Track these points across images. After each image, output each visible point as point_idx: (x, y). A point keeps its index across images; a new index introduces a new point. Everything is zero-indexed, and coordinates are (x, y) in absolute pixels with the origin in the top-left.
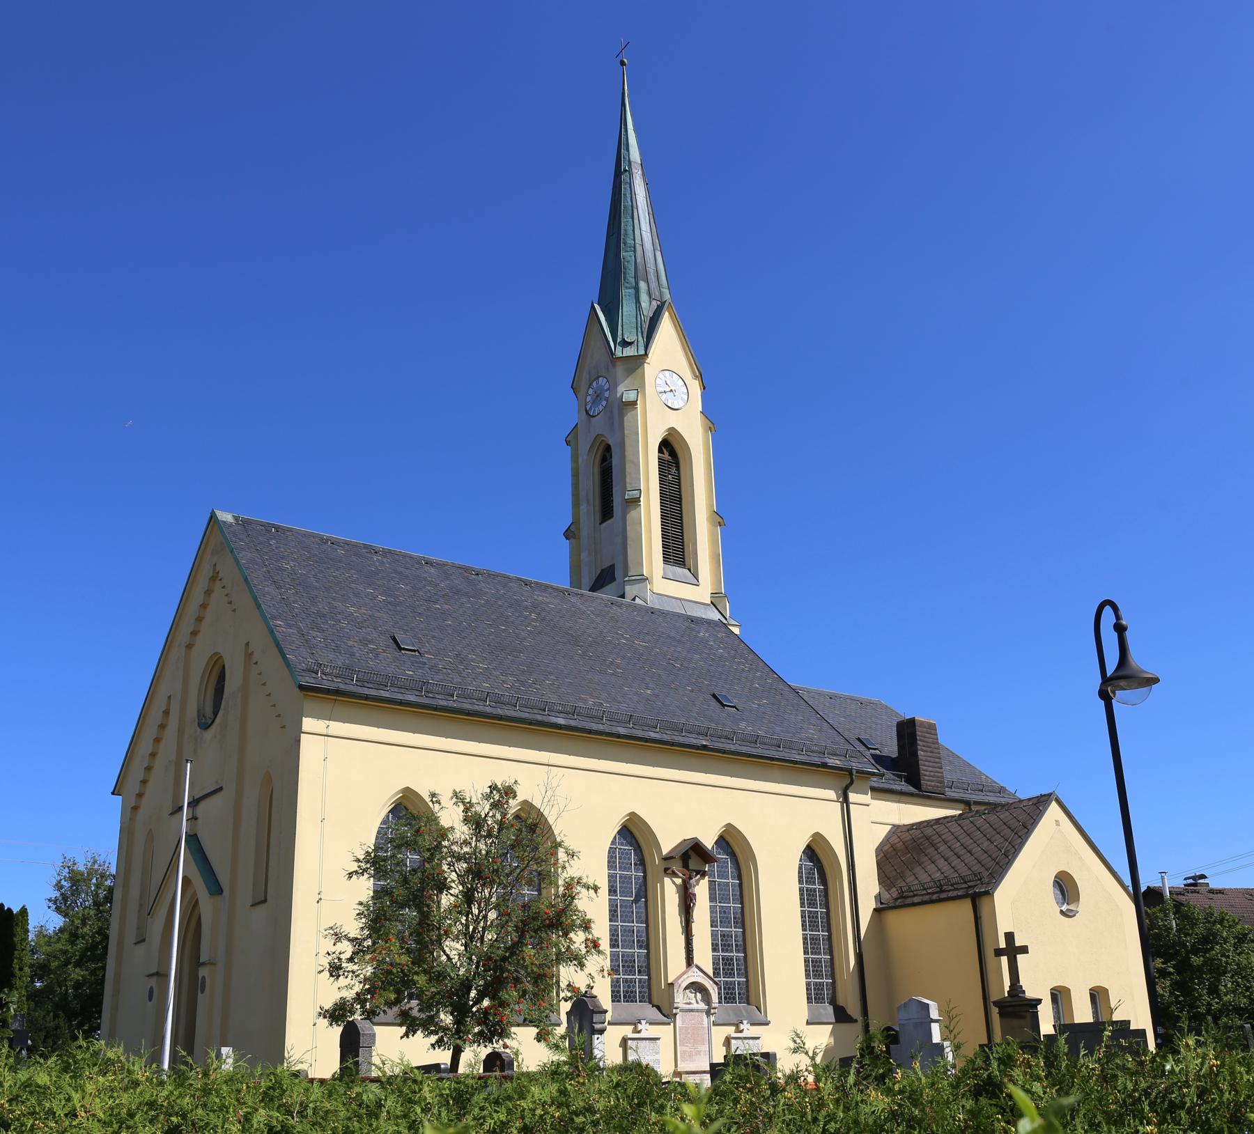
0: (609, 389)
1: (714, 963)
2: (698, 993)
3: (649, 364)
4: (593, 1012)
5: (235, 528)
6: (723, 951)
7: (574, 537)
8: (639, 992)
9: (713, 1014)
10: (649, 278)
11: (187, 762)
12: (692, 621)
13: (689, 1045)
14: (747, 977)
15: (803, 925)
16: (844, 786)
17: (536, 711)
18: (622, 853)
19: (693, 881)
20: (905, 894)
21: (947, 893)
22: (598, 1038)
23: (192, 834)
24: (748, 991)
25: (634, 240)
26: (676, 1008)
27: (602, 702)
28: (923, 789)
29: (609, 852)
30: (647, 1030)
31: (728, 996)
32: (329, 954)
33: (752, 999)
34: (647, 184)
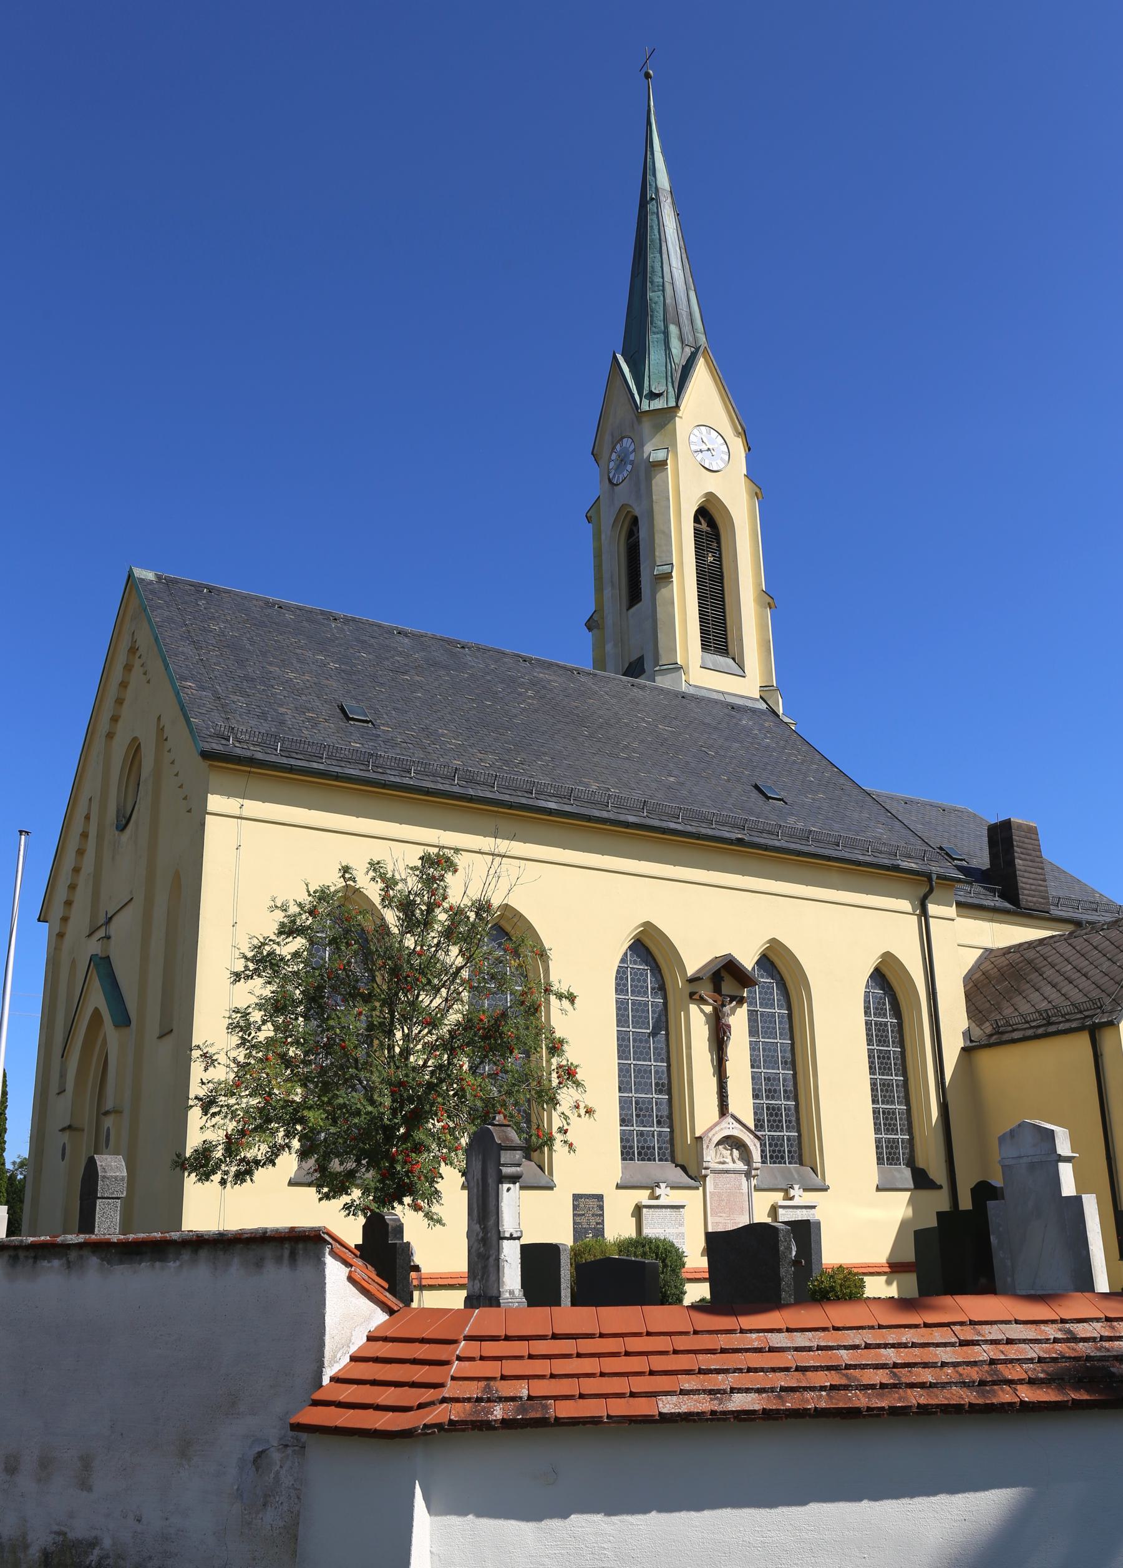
0: (634, 450)
1: (755, 1113)
2: (734, 1150)
3: (681, 417)
4: (501, 1148)
5: (156, 586)
6: (767, 1098)
7: (598, 627)
8: (659, 1148)
9: (754, 1177)
10: (681, 321)
11: (21, 835)
12: (733, 708)
13: (724, 1215)
14: (799, 1131)
15: (870, 1068)
16: (922, 895)
17: (519, 794)
18: (636, 974)
19: (727, 1009)
20: (1001, 1029)
21: (1057, 1026)
22: (508, 1190)
23: (103, 956)
24: (800, 1148)
25: (663, 278)
26: (706, 1168)
27: (610, 787)
28: (1022, 906)
29: (618, 972)
30: (668, 1196)
31: (774, 1154)
32: (203, 1083)
33: (806, 1157)
34: (678, 215)
